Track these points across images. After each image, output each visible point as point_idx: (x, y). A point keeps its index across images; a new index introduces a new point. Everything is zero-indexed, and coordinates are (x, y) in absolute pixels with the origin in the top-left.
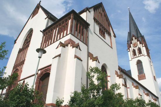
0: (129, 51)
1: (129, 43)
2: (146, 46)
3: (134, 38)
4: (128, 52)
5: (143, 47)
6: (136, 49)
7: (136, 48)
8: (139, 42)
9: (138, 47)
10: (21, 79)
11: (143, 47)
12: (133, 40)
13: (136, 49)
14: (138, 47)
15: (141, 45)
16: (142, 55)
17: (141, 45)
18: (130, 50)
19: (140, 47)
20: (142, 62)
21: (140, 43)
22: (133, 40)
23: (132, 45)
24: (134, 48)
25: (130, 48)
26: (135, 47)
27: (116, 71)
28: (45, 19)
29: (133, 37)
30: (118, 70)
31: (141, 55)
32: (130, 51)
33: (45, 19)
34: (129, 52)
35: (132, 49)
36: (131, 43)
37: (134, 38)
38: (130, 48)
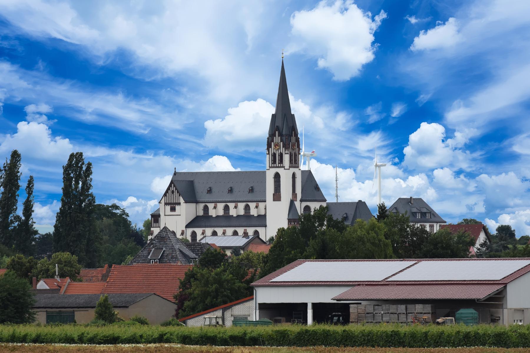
36: (273, 141)
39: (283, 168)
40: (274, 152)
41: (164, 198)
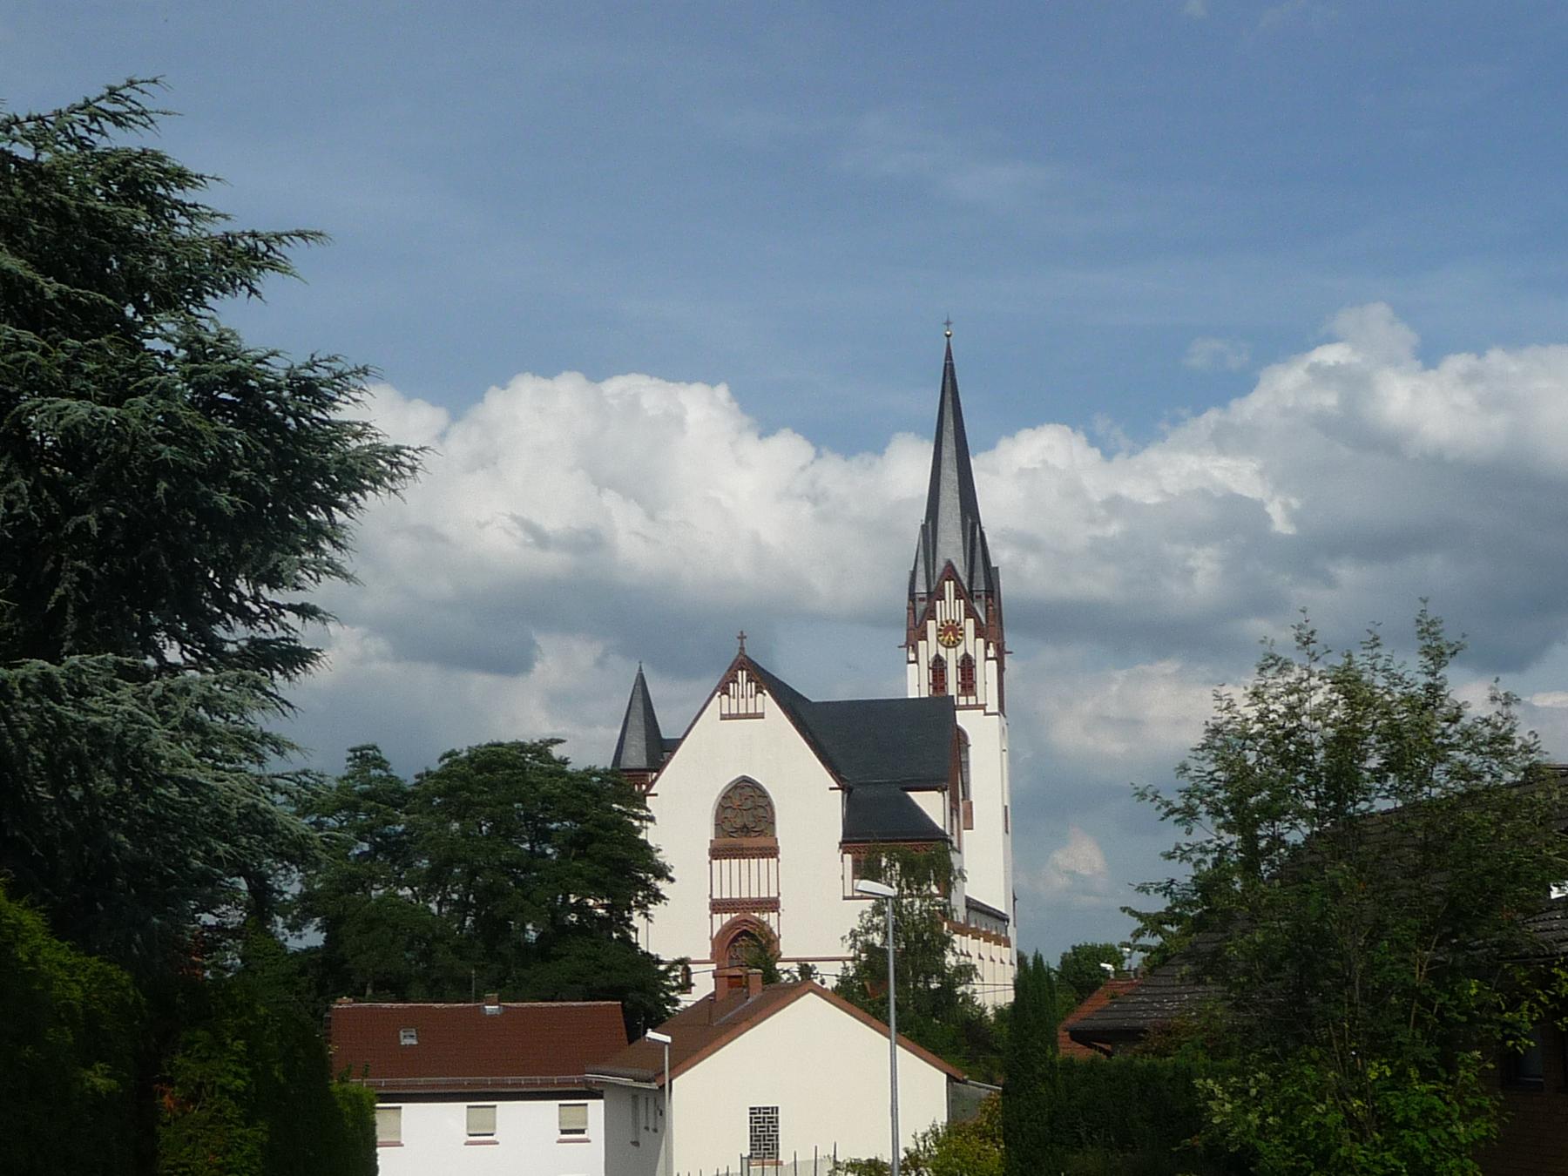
9: (961, 652)
19: (971, 653)
22: (942, 598)
40: (937, 655)
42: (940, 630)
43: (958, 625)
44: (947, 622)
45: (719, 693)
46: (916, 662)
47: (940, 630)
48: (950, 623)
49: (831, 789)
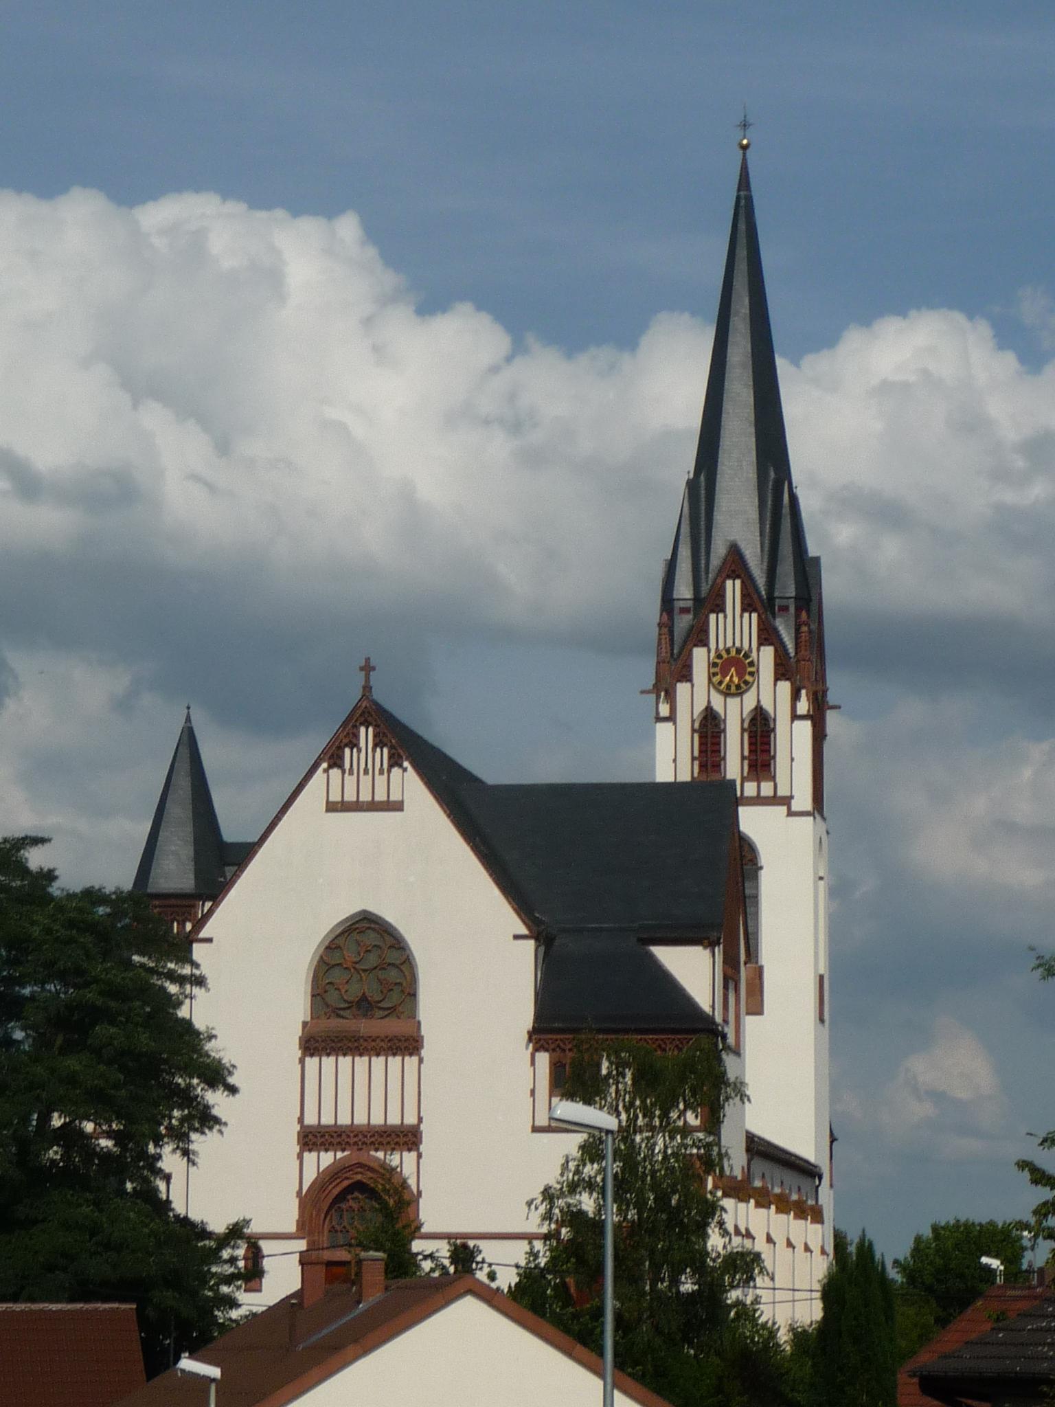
0: (664, 710)
1: (683, 622)
2: (817, 718)
3: (733, 590)
4: (659, 719)
5: (795, 717)
6: (734, 713)
7: (733, 703)
8: (766, 657)
9: (750, 701)
10: (711, 1014)
11: (797, 723)
12: (720, 608)
13: (734, 713)
14: (750, 701)
15: (785, 687)
16: (775, 800)
17: (785, 687)
18: (673, 710)
19: (767, 705)
20: (764, 858)
21: (782, 672)
22: (720, 608)
23: (700, 658)
24: (717, 702)
25: (682, 689)
26: (727, 694)
27: (1023, 1165)
28: (209, 940)
29: (733, 576)
30: (891, 1263)
31: (767, 789)
32: (672, 718)
33: (209, 940)
34: (664, 730)
35: (700, 707)
36: (699, 636)
37: (733, 590)
38: (682, 689)
39: (785, 808)
41: (319, 775)
42: (715, 665)
43: (747, 656)
44: (728, 651)
45: (325, 765)
46: (672, 718)
47: (715, 665)
48: (733, 653)
49: (516, 937)
